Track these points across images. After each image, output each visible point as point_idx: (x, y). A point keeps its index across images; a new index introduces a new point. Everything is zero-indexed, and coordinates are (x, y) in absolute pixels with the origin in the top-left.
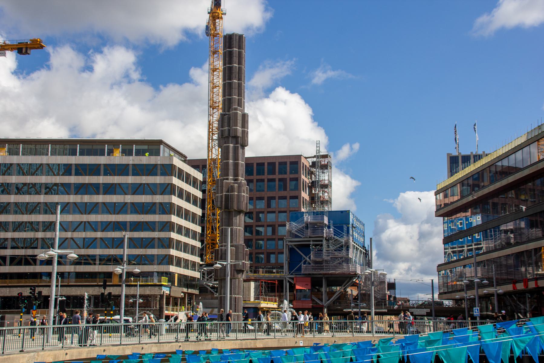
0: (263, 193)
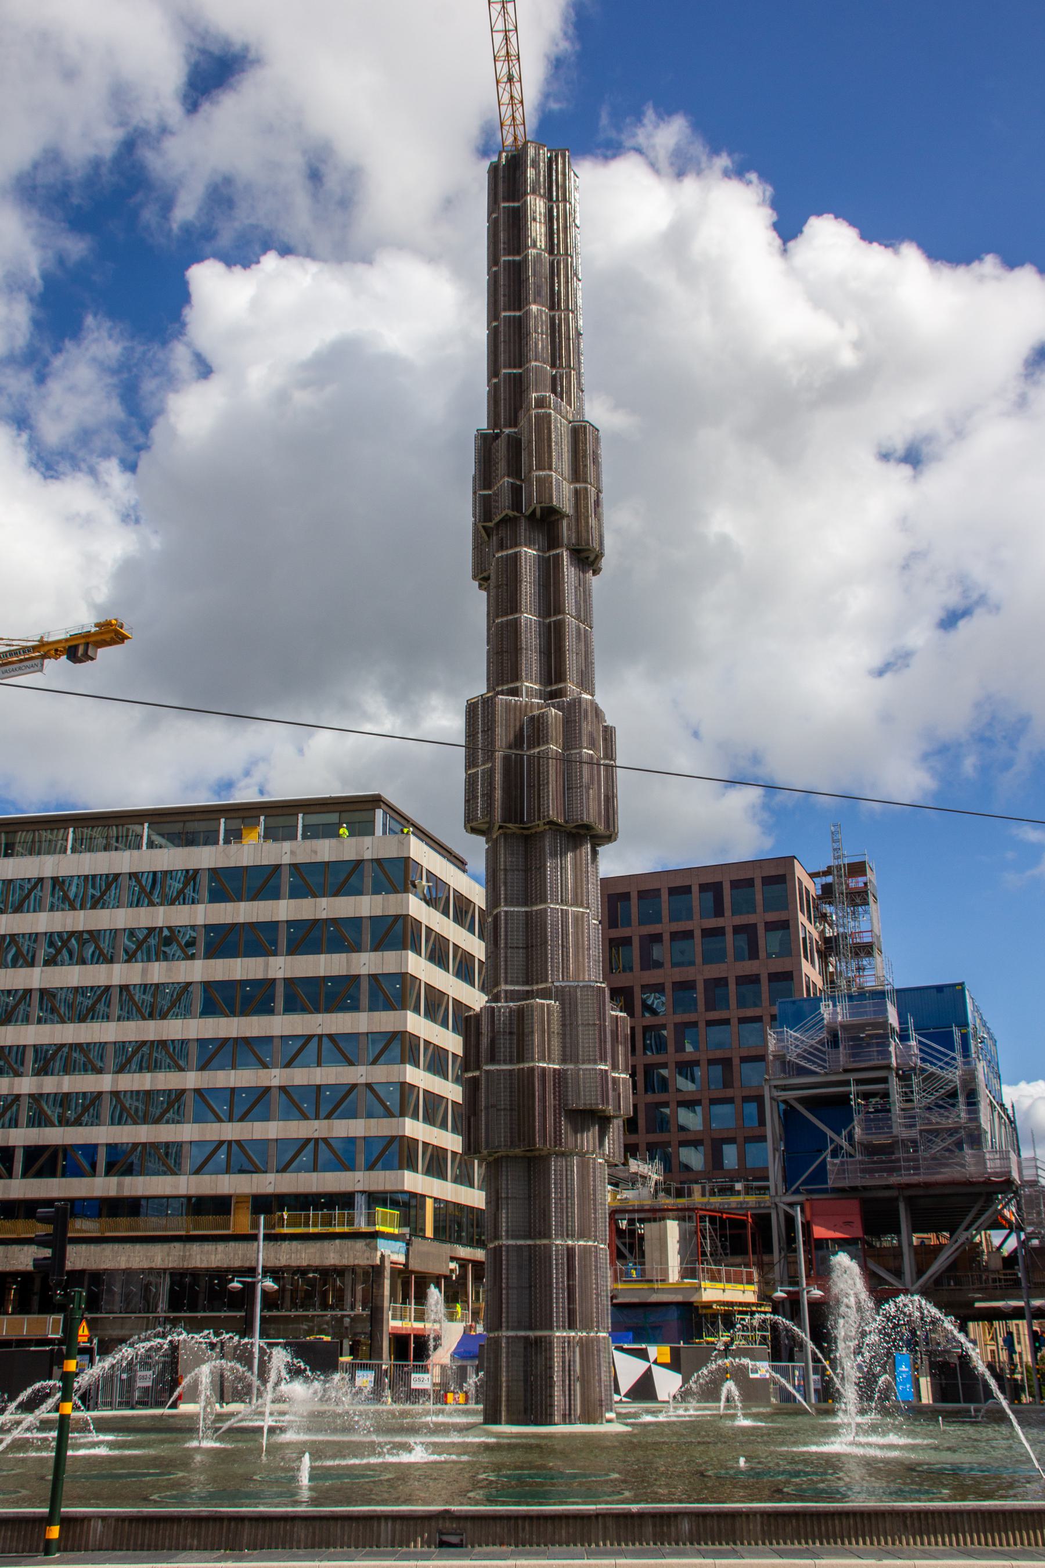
0: (691, 969)
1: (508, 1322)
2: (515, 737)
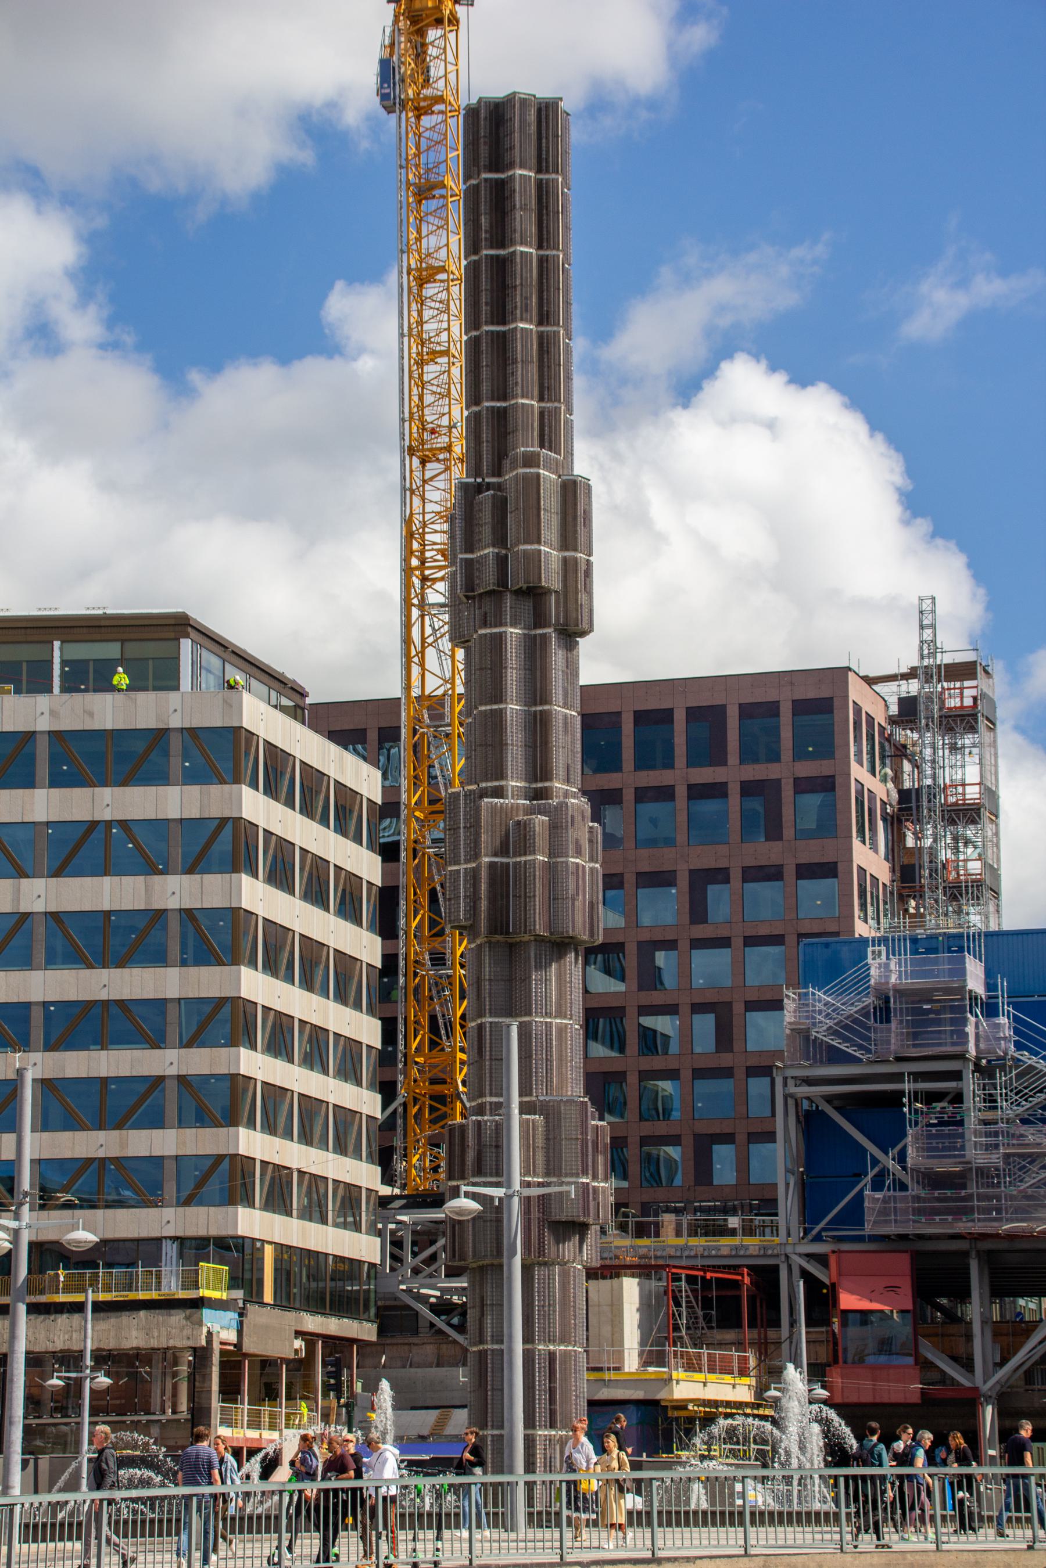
1: (493, 1421)
2: (501, 843)
